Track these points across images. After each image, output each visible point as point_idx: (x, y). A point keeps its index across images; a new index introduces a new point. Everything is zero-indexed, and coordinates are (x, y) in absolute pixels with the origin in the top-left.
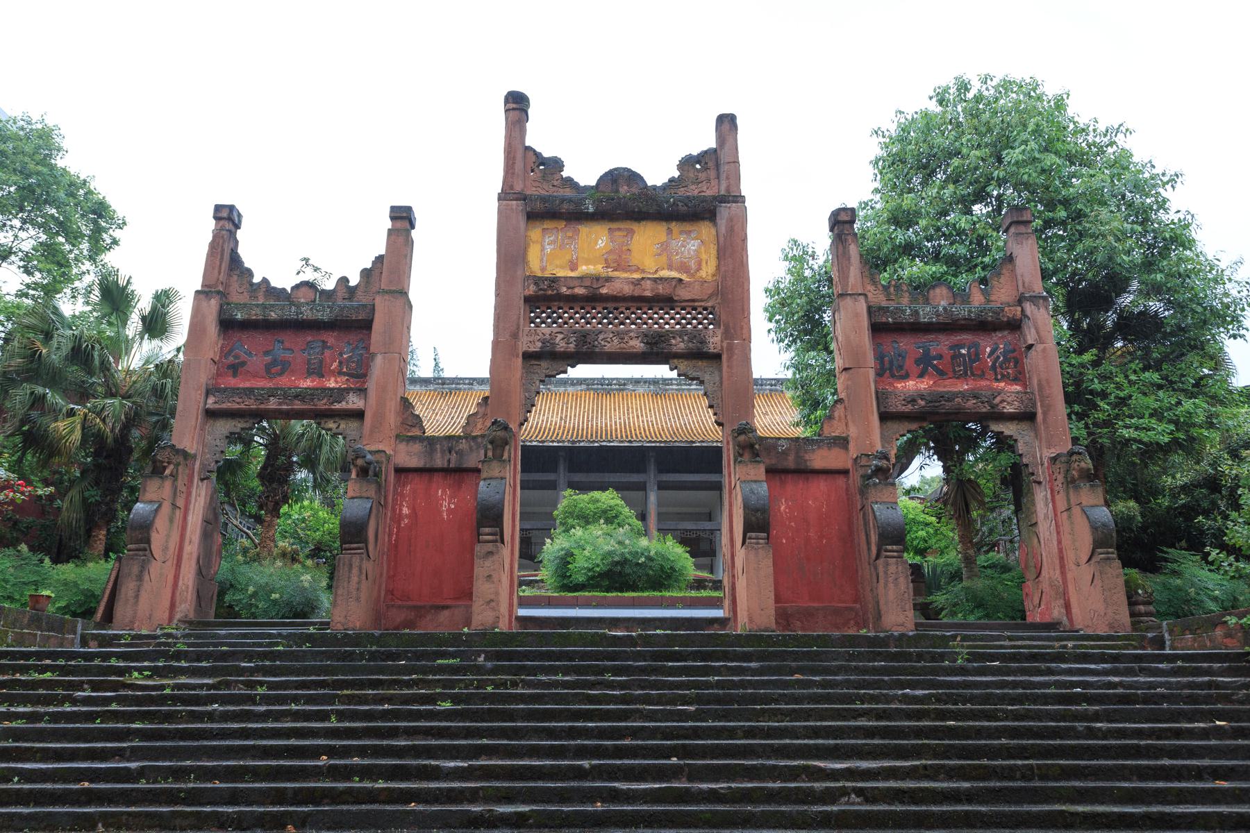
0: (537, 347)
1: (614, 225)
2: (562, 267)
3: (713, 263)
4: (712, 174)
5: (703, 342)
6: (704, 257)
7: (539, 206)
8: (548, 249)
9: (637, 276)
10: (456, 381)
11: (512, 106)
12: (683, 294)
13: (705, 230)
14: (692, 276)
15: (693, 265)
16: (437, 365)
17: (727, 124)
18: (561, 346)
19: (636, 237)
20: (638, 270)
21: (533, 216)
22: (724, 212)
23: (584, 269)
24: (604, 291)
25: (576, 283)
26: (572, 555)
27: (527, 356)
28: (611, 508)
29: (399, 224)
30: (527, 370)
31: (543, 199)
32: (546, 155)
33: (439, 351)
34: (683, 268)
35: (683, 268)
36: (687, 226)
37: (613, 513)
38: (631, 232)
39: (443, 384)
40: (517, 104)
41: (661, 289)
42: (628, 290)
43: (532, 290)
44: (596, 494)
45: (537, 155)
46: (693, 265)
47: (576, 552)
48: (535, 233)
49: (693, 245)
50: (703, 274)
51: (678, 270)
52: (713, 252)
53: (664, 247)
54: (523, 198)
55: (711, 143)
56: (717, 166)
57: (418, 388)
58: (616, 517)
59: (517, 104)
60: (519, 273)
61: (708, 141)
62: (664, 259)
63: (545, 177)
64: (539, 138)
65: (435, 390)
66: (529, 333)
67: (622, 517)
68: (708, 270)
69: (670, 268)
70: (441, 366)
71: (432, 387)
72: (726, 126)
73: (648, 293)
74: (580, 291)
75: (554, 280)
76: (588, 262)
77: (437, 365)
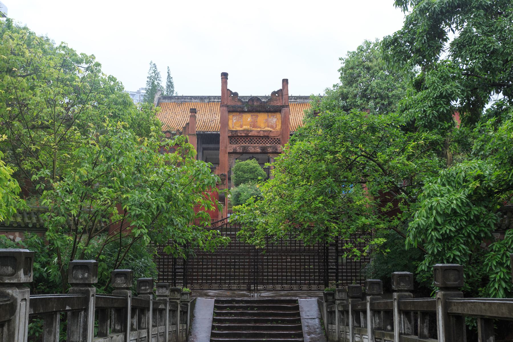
0: (232, 151)
1: (253, 114)
2: (238, 127)
3: (280, 125)
4: (280, 97)
5: (276, 149)
6: (278, 123)
7: (231, 109)
8: (234, 121)
9: (259, 129)
10: (183, 97)
11: (223, 77)
12: (271, 135)
13: (278, 115)
14: (274, 129)
15: (275, 126)
16: (169, 75)
17: (285, 82)
18: (238, 151)
19: (259, 118)
20: (259, 127)
21: (229, 112)
22: (284, 110)
23: (245, 127)
24: (250, 134)
25: (241, 132)
26: (240, 194)
27: (229, 153)
28: (254, 167)
29: (193, 114)
30: (229, 157)
31: (233, 107)
32: (233, 92)
33: (170, 68)
34: (272, 127)
35: (272, 127)
36: (273, 114)
37: (254, 170)
38: (258, 116)
39: (178, 99)
40: (225, 76)
41: (266, 134)
42: (256, 134)
43: (230, 134)
44: (248, 161)
45: (231, 92)
46: (275, 126)
47: (241, 193)
48: (231, 116)
49: (275, 120)
50: (277, 128)
51: (271, 127)
52: (280, 122)
53: (267, 120)
54: (227, 106)
55: (280, 87)
56: (282, 95)
57: (167, 101)
58: (256, 171)
59: (225, 76)
60: (227, 129)
61: (279, 87)
62: (266, 124)
63: (233, 98)
64: (232, 86)
65: (175, 102)
66: (230, 147)
67: (258, 171)
68: (279, 127)
69: (268, 127)
70: (171, 76)
71: (173, 101)
72: (285, 83)
73: (262, 135)
74: (243, 134)
75: (236, 131)
76: (245, 125)
77: (169, 75)
